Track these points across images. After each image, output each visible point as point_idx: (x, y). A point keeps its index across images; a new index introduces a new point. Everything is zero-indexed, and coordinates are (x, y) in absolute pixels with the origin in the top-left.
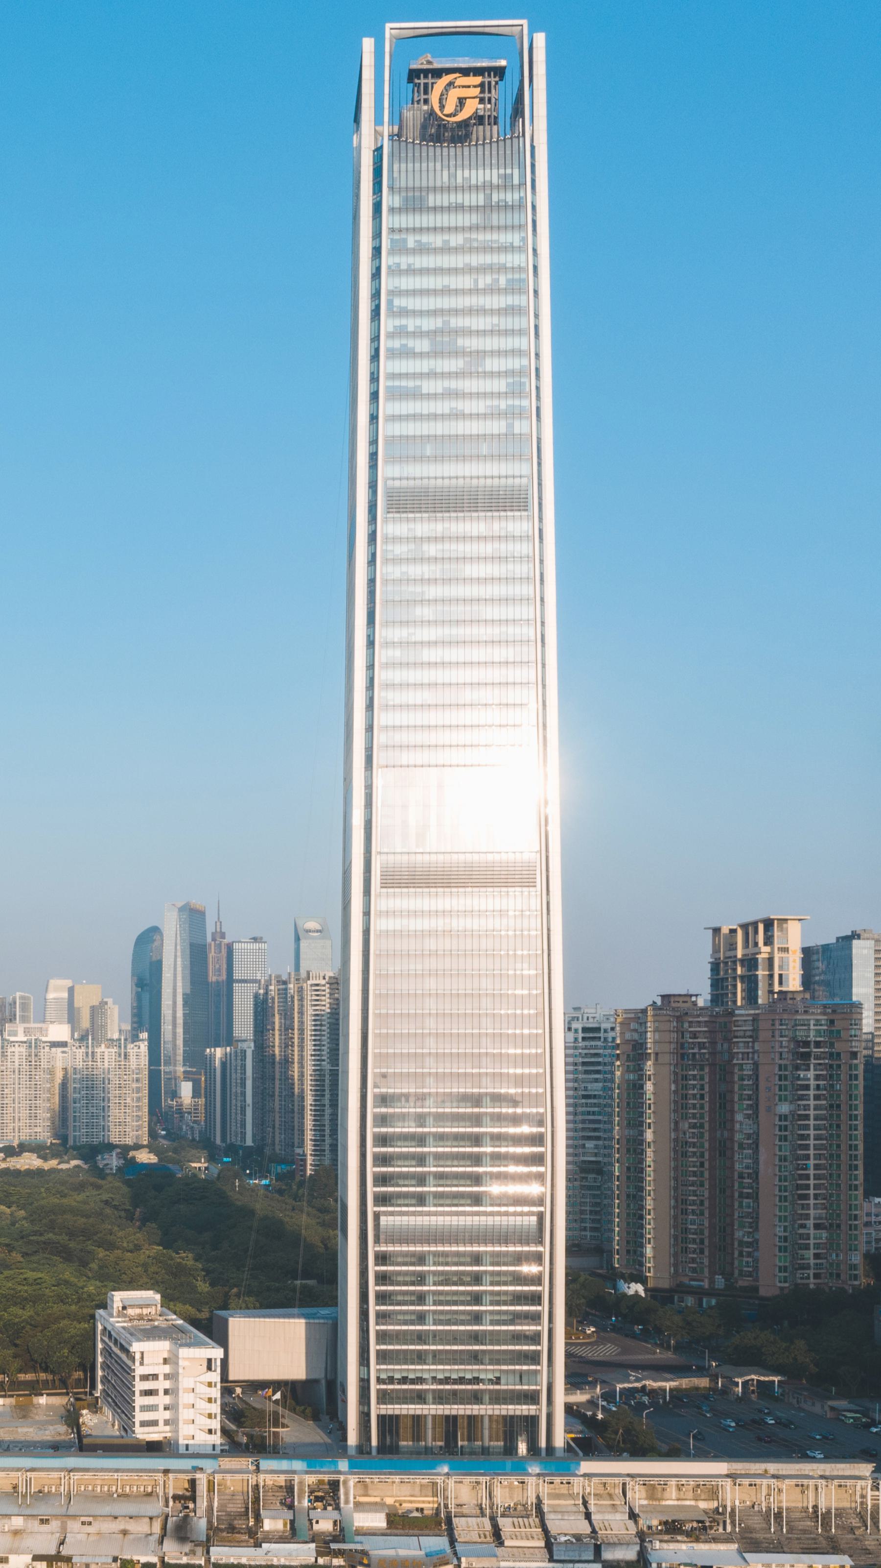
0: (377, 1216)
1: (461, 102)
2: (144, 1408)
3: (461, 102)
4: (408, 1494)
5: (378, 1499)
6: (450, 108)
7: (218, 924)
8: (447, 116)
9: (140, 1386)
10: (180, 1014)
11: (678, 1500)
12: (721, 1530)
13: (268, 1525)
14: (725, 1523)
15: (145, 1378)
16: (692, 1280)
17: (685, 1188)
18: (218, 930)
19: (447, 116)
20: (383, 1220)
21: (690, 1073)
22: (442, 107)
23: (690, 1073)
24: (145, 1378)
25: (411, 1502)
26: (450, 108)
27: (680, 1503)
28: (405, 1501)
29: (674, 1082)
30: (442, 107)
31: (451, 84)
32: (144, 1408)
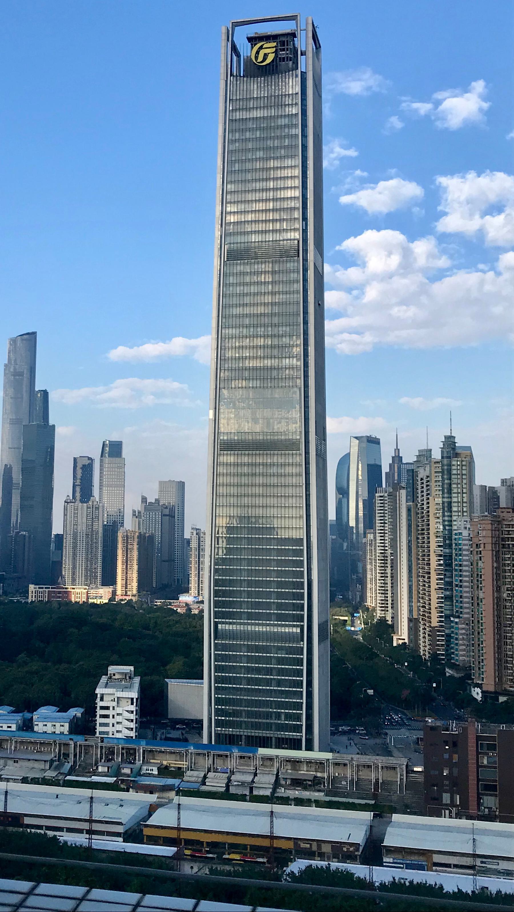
1: (266, 56)
2: (101, 725)
3: (266, 56)
4: (174, 759)
5: (159, 761)
6: (260, 59)
7: (397, 451)
8: (258, 63)
9: (99, 712)
10: (361, 513)
11: (307, 771)
12: (322, 786)
13: (100, 769)
14: (324, 783)
15: (102, 708)
16: (511, 687)
17: (505, 628)
18: (397, 455)
19: (258, 63)
20: (220, 626)
21: (506, 556)
23: (506, 556)
24: (102, 708)
25: (175, 764)
26: (260, 59)
27: (308, 773)
28: (172, 763)
29: (496, 561)
30: (256, 60)
31: (261, 48)
32: (101, 725)
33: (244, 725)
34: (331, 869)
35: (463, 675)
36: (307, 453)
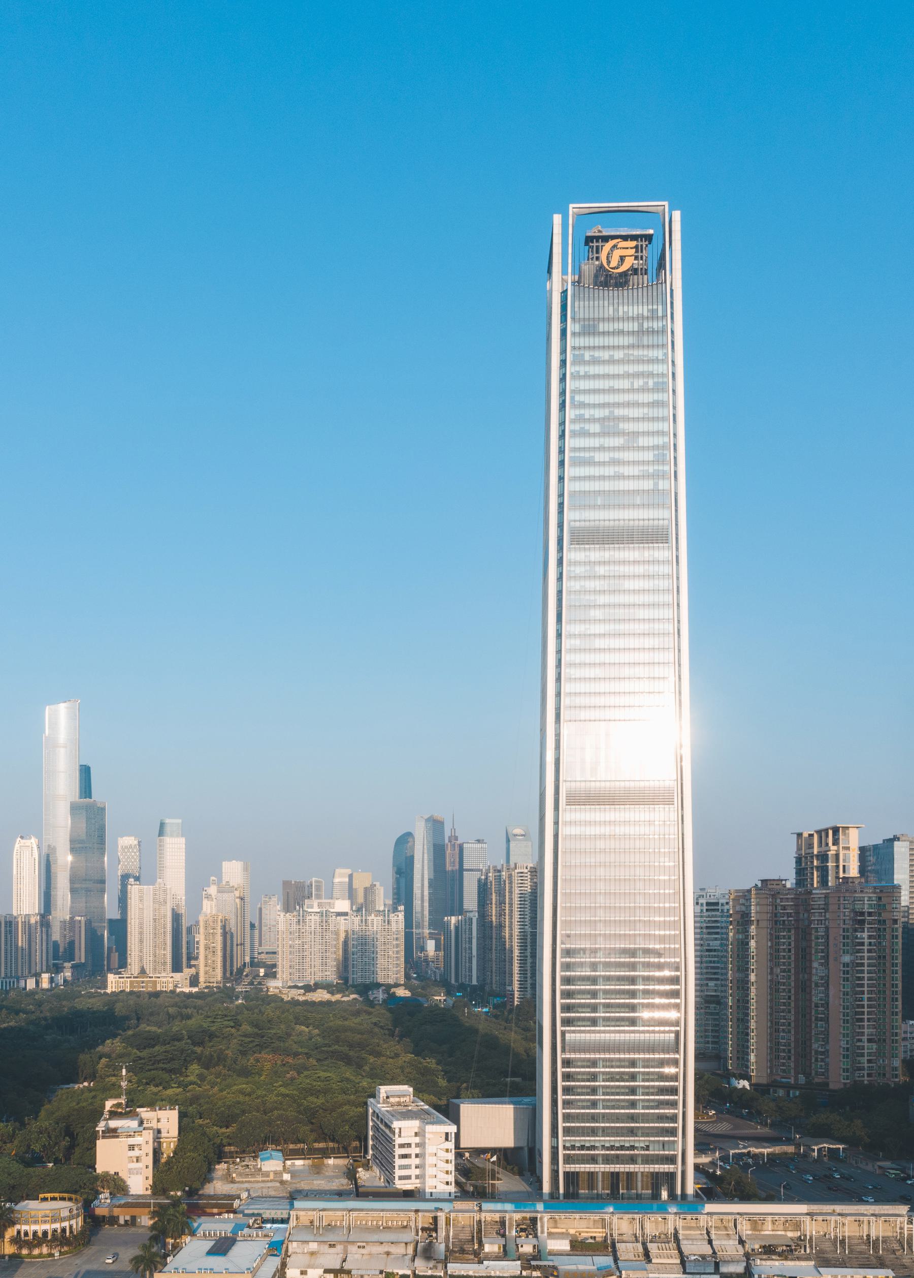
0: (563, 1033)
1: (622, 259)
2: (402, 1167)
3: (622, 259)
5: (564, 1230)
6: (614, 263)
9: (398, 1151)
12: (803, 1252)
13: (487, 1248)
14: (805, 1246)
15: (402, 1146)
22: (609, 262)
24: (402, 1146)
25: (587, 1232)
26: (614, 263)
27: (774, 1233)
31: (615, 246)
32: (402, 1167)
33: (639, 1160)
34: (152, 1222)
35: (905, 899)
36: (560, 526)
